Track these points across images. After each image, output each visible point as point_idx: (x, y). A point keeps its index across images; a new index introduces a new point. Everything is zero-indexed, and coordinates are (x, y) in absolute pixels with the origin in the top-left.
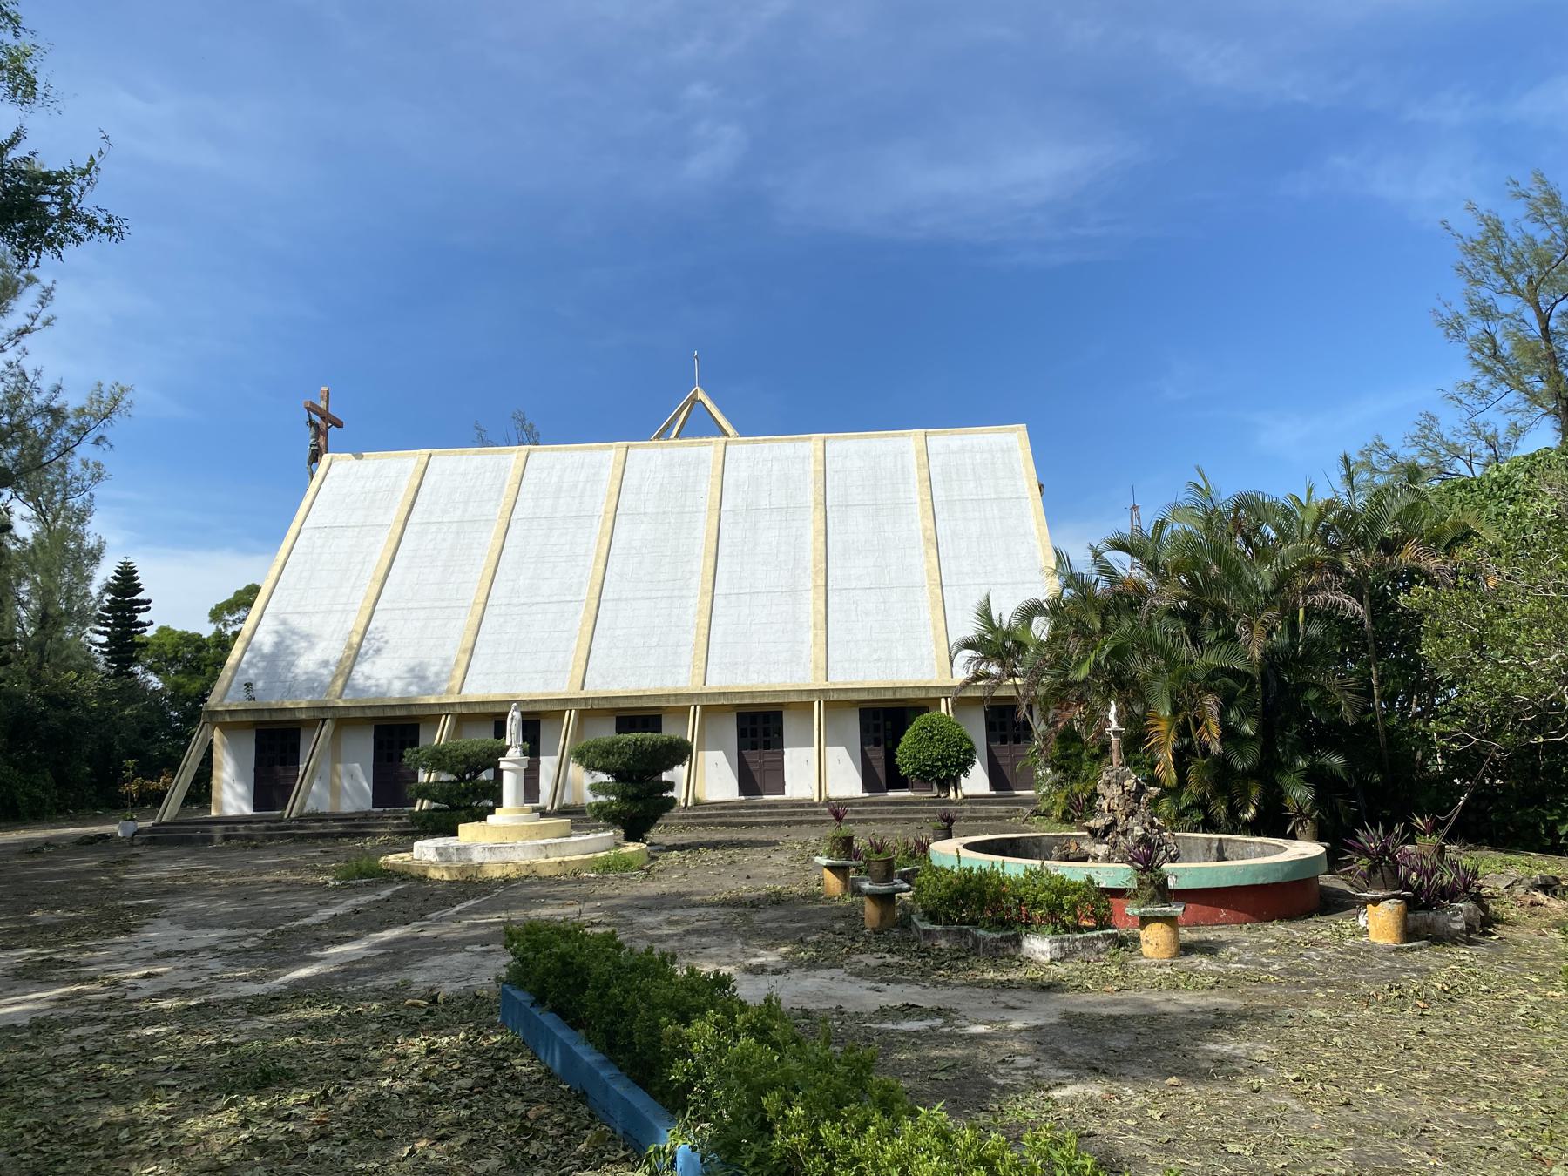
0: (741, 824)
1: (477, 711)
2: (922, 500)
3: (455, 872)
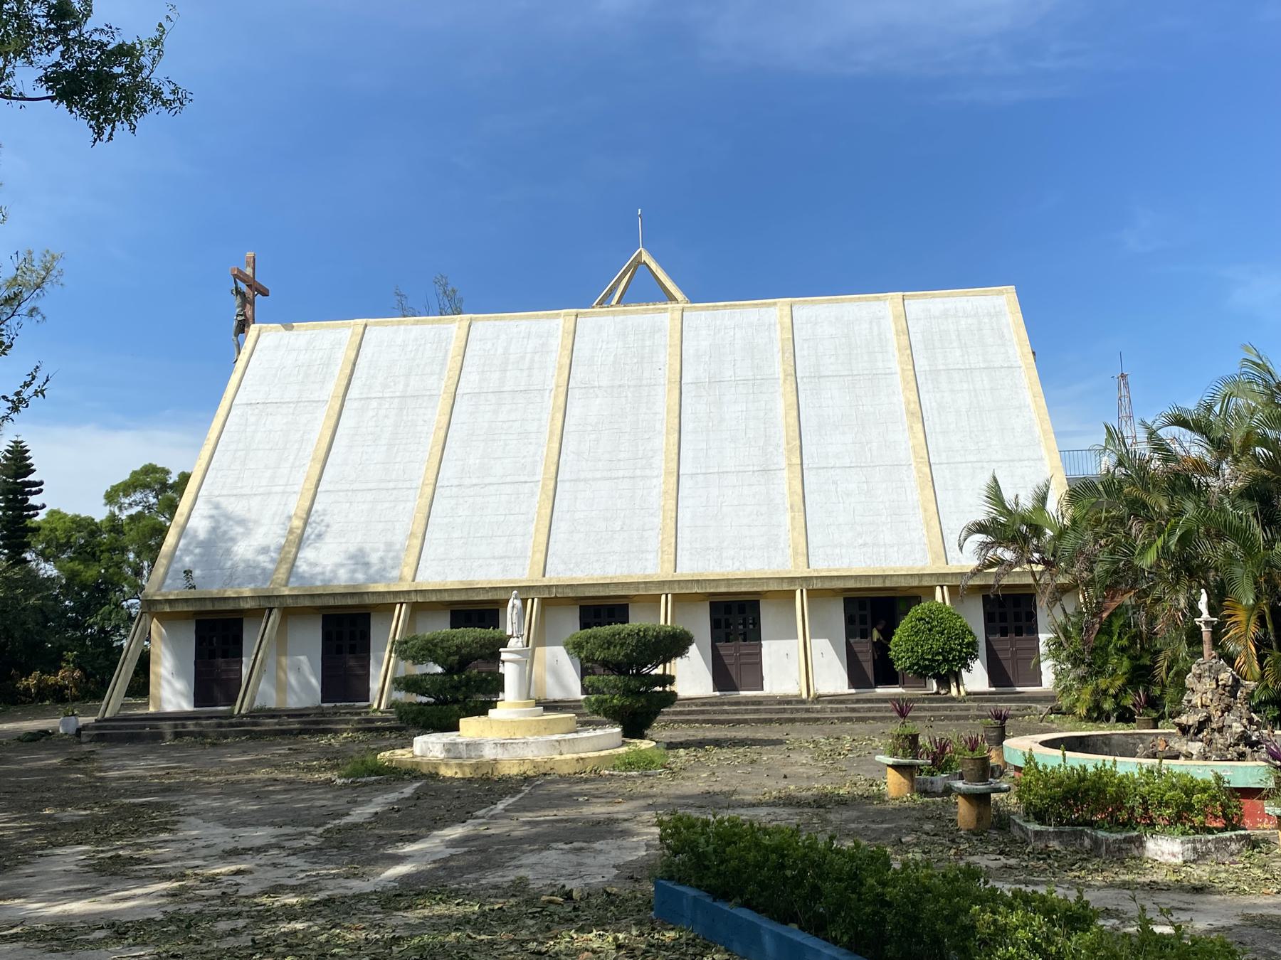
0: (728, 722)
1: (434, 599)
2: (903, 370)
3: (467, 770)
